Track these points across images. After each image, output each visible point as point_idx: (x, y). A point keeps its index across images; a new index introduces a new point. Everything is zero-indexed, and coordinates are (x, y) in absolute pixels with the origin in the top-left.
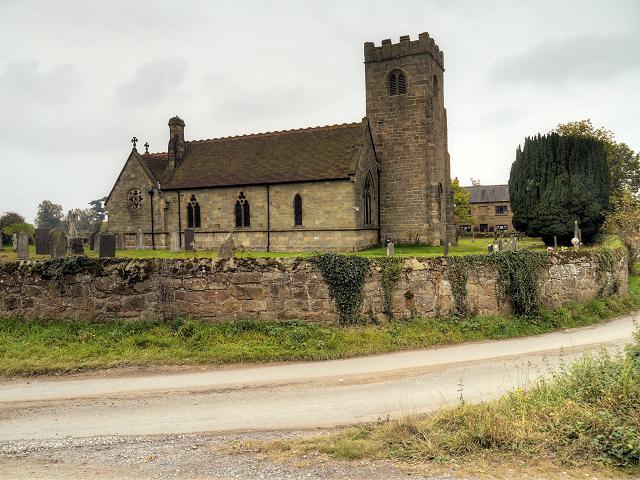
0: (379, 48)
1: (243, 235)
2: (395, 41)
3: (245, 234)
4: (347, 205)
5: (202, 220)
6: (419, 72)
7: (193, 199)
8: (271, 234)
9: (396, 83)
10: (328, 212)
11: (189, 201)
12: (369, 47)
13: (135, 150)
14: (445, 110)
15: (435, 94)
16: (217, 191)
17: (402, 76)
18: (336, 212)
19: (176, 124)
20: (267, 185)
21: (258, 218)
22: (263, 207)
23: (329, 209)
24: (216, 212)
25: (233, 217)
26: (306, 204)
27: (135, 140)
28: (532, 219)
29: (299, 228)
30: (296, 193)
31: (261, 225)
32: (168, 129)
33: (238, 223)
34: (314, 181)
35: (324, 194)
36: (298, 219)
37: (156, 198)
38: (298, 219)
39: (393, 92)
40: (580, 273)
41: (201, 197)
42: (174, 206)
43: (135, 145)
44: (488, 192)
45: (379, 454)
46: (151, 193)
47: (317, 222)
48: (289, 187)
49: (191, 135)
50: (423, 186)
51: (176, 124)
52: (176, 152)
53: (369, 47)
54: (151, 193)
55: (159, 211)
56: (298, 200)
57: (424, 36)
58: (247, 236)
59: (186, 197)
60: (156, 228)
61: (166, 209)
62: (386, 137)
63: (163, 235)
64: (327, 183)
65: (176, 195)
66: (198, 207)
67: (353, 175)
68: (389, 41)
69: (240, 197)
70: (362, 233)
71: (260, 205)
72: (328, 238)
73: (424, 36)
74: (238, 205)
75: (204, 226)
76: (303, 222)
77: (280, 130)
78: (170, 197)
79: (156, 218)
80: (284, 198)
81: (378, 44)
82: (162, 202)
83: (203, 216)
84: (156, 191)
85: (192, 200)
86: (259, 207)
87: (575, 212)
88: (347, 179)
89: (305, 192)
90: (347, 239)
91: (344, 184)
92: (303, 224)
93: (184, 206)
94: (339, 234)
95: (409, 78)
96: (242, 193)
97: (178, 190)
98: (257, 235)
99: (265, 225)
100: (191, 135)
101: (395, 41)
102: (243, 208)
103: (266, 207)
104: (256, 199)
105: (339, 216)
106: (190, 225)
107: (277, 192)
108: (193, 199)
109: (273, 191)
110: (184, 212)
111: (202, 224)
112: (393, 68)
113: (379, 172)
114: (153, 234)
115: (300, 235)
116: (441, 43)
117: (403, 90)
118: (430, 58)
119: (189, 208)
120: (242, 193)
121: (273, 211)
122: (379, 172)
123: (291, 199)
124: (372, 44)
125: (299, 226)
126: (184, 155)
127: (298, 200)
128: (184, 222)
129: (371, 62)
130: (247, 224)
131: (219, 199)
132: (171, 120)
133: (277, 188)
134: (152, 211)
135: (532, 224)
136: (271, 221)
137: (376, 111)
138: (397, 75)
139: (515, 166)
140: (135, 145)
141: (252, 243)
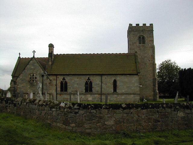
2: (141, 25)
3: (90, 95)
7: (64, 79)
9: (142, 40)
11: (62, 80)
12: (130, 25)
16: (77, 76)
18: (132, 87)
19: (51, 46)
20: (101, 75)
21: (96, 88)
22: (99, 84)
23: (128, 86)
24: (76, 85)
26: (118, 83)
29: (115, 93)
30: (113, 79)
31: (98, 91)
32: (48, 48)
33: (86, 90)
35: (126, 80)
39: (140, 43)
41: (67, 79)
42: (54, 83)
43: (34, 54)
46: (43, 76)
47: (123, 91)
50: (152, 78)
51: (51, 46)
53: (130, 25)
54: (43, 76)
56: (115, 82)
59: (60, 78)
64: (128, 76)
65: (55, 77)
66: (66, 83)
69: (88, 80)
71: (98, 83)
74: (86, 83)
75: (69, 91)
77: (96, 53)
78: (51, 78)
80: (109, 80)
83: (68, 87)
85: (63, 80)
86: (97, 84)
88: (137, 74)
90: (136, 97)
91: (135, 76)
94: (132, 96)
96: (64, 78)
97: (56, 75)
98: (96, 96)
100: (55, 52)
101: (141, 25)
103: (100, 84)
104: (96, 81)
105: (133, 88)
108: (64, 79)
109: (104, 77)
114: (101, 94)
115: (115, 96)
116: (137, 23)
117: (144, 43)
119: (62, 83)
120: (89, 78)
121: (104, 86)
123: (112, 81)
124: (132, 25)
127: (115, 82)
128: (59, 89)
130: (91, 90)
131: (78, 80)
132: (53, 45)
133: (106, 76)
139: (44, 58)
140: (34, 54)
141: (93, 99)
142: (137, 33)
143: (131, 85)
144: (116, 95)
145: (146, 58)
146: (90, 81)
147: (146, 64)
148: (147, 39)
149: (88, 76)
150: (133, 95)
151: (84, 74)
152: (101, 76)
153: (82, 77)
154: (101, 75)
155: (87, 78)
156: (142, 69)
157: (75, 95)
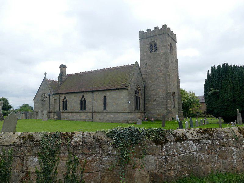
0: (145, 33)
1: (83, 114)
2: (152, 29)
4: (125, 100)
5: (68, 107)
6: (162, 42)
7: (65, 98)
8: (93, 113)
10: (117, 104)
11: (63, 99)
12: (141, 33)
13: (45, 78)
14: (177, 60)
15: (171, 52)
16: (74, 95)
17: (155, 45)
19: (63, 67)
20: (93, 92)
21: (89, 106)
22: (91, 101)
25: (79, 106)
26: (108, 100)
27: (45, 74)
28: (215, 108)
31: (90, 109)
32: (59, 69)
33: (81, 109)
34: (111, 90)
36: (105, 107)
37: (51, 97)
38: (105, 107)
40: (201, 150)
42: (58, 101)
43: (45, 76)
46: (50, 95)
48: (101, 92)
49: (69, 72)
51: (63, 67)
52: (61, 78)
54: (50, 95)
55: (52, 103)
56: (105, 98)
57: (165, 26)
58: (85, 114)
59: (62, 97)
60: (51, 110)
61: (55, 102)
62: (148, 71)
63: (53, 113)
67: (128, 86)
68: (150, 30)
70: (133, 114)
71: (90, 100)
72: (117, 116)
73: (165, 26)
74: (81, 101)
76: (107, 108)
78: (57, 97)
79: (51, 106)
80: (99, 97)
81: (145, 31)
82: (53, 99)
83: (68, 105)
84: (51, 95)
87: (238, 104)
88: (125, 89)
89: (108, 94)
91: (124, 91)
93: (61, 101)
94: (121, 114)
95: (158, 45)
96: (83, 95)
97: (59, 94)
98: (88, 114)
99: (92, 109)
101: (152, 29)
102: (83, 101)
104: (88, 97)
106: (63, 109)
107: (96, 95)
108: (65, 98)
109: (95, 94)
110: (62, 103)
111: (67, 109)
112: (151, 41)
113: (145, 86)
115: (105, 114)
117: (156, 50)
118: (167, 36)
119: (63, 102)
120: (83, 95)
122: (145, 86)
123: (103, 98)
125: (105, 110)
126: (66, 80)
127: (105, 98)
128: (61, 108)
129: (142, 39)
130: (85, 109)
131: (74, 98)
134: (49, 103)
135: (216, 111)
138: (153, 44)
140: (45, 76)
146: (84, 98)
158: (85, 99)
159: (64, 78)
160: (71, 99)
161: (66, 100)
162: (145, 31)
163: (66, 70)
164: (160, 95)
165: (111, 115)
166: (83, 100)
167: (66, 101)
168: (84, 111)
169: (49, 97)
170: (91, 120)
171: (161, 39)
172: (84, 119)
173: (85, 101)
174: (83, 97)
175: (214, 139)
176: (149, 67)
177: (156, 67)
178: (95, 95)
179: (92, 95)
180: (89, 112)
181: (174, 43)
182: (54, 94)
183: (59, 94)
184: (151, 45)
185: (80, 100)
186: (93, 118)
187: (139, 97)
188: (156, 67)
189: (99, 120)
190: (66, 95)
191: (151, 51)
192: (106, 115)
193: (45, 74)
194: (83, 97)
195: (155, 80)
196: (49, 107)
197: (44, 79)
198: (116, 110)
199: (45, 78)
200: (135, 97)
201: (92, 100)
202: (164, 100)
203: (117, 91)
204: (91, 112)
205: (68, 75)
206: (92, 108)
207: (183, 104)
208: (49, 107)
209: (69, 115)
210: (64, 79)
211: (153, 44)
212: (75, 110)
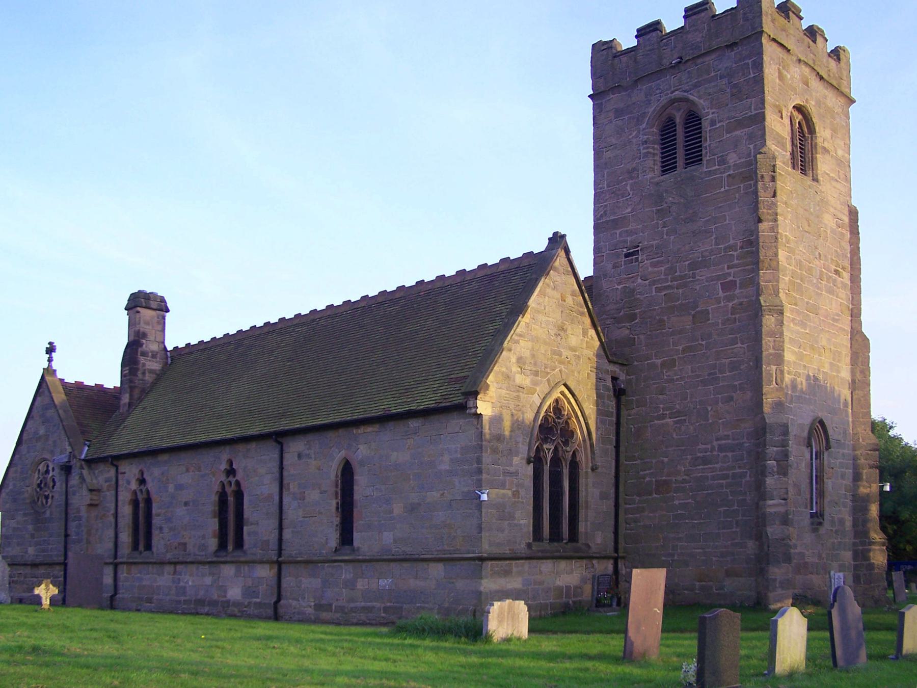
1: (228, 571)
8: (284, 566)
11: (134, 486)
13: (49, 371)
16: (187, 458)
17: (693, 120)
24: (181, 511)
26: (362, 487)
27: (51, 349)
33: (223, 545)
37: (74, 480)
41: (154, 472)
43: (50, 360)
44: (533, 614)
45: (549, 447)
46: (67, 469)
54: (67, 469)
56: (347, 472)
59: (130, 471)
68: (656, 26)
72: (413, 583)
77: (305, 311)
78: (105, 474)
81: (627, 41)
83: (156, 521)
92: (356, 543)
93: (125, 496)
94: (437, 570)
95: (708, 115)
96: (231, 463)
99: (274, 544)
106: (135, 546)
109: (295, 447)
110: (126, 510)
112: (664, 100)
114: (116, 566)
115: (346, 572)
119: (135, 503)
120: (231, 463)
123: (333, 470)
126: (160, 376)
127: (347, 472)
128: (125, 537)
130: (239, 544)
136: (287, 534)
137: (616, 223)
138: (679, 119)
140: (50, 360)
141: (249, 592)
142: (638, 96)
143: (433, 496)
144: (350, 567)
145: (703, 274)
146: (233, 480)
147: (701, 317)
148: (713, 123)
149: (225, 454)
150: (440, 566)
151: (228, 435)
152: (271, 445)
153: (207, 457)
154: (279, 437)
155: (224, 466)
156: (673, 363)
157: (179, 567)
158: (238, 483)
159: (155, 365)
160: (171, 489)
161: (148, 492)
162: (627, 41)
163: (162, 323)
164: (715, 443)
165: (507, 573)
166: (229, 490)
167: (148, 501)
168: (147, 553)
169: (64, 478)
170: (270, 612)
171: (725, 81)
172: (237, 604)
173: (239, 495)
174: (231, 472)
175: (842, 299)
176: (654, 265)
177: (694, 266)
178: (290, 458)
179: (276, 456)
180: (262, 562)
181: (833, 100)
182: (90, 462)
183: (115, 460)
184: (667, 130)
185: (217, 488)
186: (279, 599)
187: (574, 465)
188: (694, 266)
189: (310, 611)
190: (149, 460)
191: (668, 166)
192: (349, 576)
193: (51, 349)
194: (231, 472)
195: (684, 351)
196: (66, 536)
197: (43, 377)
198: (408, 549)
199: (49, 371)
200: (536, 460)
201: (275, 489)
202: (743, 475)
203: (414, 423)
204: (271, 562)
205: (176, 348)
206: (274, 536)
207: (557, 408)
208: (66, 536)
209: (163, 580)
210: (149, 378)
211: (679, 119)
212: (190, 548)
